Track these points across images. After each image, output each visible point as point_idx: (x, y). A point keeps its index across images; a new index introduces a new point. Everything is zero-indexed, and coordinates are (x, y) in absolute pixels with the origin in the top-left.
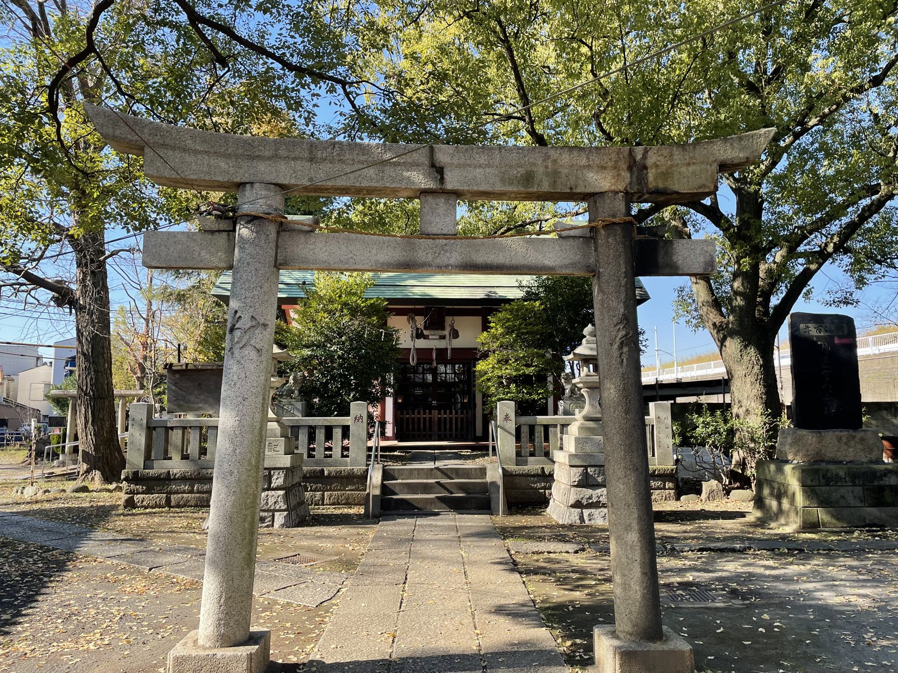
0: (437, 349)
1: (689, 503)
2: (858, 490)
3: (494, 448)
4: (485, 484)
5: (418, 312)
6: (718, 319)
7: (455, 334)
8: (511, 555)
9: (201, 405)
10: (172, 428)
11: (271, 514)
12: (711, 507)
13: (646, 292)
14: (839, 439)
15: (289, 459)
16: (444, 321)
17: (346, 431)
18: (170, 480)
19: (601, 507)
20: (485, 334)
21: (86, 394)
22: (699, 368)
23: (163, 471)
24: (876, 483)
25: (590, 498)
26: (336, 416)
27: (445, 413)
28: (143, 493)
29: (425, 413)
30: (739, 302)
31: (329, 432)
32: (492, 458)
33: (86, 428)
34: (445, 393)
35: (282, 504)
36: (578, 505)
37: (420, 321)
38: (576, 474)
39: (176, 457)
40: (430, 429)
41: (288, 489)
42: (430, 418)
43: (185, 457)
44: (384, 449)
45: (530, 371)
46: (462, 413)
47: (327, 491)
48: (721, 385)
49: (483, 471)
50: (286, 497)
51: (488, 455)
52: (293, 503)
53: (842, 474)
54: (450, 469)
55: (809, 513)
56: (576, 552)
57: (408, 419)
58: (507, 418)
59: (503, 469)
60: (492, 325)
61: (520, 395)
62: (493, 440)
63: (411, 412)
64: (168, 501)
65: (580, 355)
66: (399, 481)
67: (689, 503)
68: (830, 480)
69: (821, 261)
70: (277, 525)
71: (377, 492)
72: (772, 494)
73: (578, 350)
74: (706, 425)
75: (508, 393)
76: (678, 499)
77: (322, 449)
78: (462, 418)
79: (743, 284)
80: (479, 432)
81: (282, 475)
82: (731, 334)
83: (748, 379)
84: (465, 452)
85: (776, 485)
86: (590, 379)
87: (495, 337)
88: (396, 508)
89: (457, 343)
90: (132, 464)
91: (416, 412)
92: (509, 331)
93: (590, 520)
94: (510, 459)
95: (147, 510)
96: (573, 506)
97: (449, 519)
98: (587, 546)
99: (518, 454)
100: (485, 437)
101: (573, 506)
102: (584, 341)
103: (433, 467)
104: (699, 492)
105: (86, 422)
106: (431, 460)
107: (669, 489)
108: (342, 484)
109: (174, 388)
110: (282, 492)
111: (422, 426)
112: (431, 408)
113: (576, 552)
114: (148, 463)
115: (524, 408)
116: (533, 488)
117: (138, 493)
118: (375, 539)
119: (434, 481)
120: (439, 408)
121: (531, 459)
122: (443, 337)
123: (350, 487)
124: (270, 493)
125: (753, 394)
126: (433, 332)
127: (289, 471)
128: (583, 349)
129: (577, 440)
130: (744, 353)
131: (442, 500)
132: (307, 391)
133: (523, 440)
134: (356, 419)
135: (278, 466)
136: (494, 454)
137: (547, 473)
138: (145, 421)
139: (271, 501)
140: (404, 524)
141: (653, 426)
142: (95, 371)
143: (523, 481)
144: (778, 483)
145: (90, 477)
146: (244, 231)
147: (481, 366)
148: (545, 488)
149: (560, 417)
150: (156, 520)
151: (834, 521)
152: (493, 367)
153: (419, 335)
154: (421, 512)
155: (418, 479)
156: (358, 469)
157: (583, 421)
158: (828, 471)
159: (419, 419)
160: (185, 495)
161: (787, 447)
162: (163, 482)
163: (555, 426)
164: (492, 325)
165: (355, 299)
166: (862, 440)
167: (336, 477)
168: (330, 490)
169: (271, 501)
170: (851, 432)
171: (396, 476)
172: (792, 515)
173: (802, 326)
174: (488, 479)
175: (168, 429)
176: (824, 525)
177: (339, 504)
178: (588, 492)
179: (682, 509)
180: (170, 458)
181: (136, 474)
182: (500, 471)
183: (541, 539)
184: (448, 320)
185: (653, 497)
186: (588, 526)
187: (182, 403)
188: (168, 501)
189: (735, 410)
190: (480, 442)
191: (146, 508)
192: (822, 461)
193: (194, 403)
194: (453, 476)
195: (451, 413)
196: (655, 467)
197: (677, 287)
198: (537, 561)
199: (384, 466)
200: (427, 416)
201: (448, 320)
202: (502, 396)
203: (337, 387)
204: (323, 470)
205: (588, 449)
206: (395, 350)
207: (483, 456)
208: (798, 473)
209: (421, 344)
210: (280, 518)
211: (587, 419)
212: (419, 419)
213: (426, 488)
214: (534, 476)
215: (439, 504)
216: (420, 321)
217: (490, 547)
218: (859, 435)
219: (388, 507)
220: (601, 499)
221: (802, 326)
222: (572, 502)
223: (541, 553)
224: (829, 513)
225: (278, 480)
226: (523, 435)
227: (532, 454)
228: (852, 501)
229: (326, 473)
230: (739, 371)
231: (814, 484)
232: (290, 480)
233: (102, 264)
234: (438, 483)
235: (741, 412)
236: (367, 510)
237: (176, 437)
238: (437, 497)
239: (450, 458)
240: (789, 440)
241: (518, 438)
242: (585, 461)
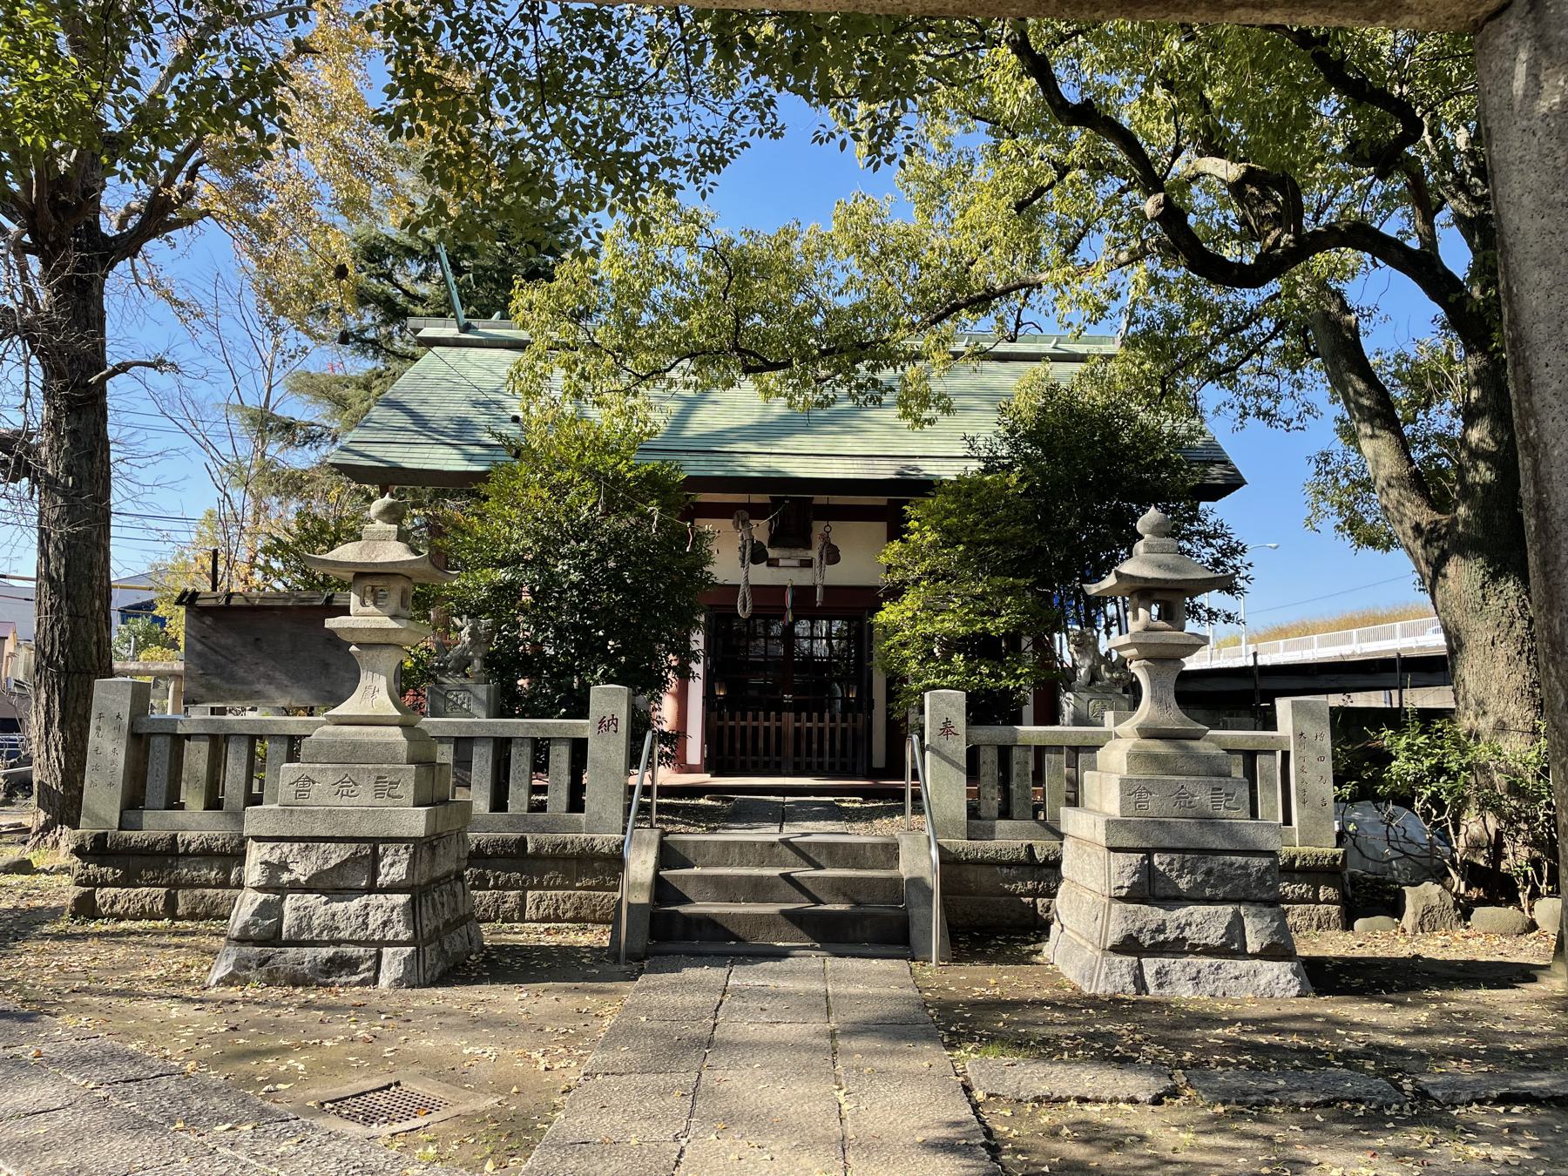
0: (794, 588)
1: (1372, 939)
3: (917, 796)
4: (896, 882)
5: (757, 512)
6: (1426, 516)
7: (832, 556)
8: (975, 1107)
9: (258, 687)
10: (188, 737)
11: (373, 951)
12: (1433, 947)
13: (1235, 470)
15: (423, 817)
16: (810, 530)
17: (579, 749)
18: (178, 856)
19: (1186, 954)
20: (897, 545)
21: (50, 664)
22: (1322, 644)
23: (162, 834)
25: (1161, 929)
26: (565, 716)
27: (809, 719)
28: (114, 884)
29: (767, 719)
30: (1483, 474)
31: (540, 751)
32: (909, 819)
33: (47, 734)
34: (813, 682)
35: (400, 927)
36: (1129, 946)
37: (761, 530)
38: (1124, 869)
39: (192, 798)
40: (778, 753)
41: (418, 892)
42: (779, 729)
45: (995, 626)
46: (844, 720)
47: (533, 888)
48: (1432, 669)
49: (890, 852)
50: (413, 909)
51: (901, 811)
52: (428, 925)
54: (816, 844)
56: (1157, 1101)
57: (732, 728)
58: (947, 729)
59: (940, 847)
60: (913, 524)
61: (975, 680)
62: (915, 776)
63: (738, 714)
64: (171, 903)
65: (1132, 577)
66: (696, 870)
67: (1372, 939)
70: (384, 981)
71: (643, 898)
73: (1127, 568)
74: (1414, 752)
75: (947, 673)
76: (1348, 926)
77: (524, 793)
78: (844, 730)
79: (1492, 432)
80: (879, 759)
81: (405, 856)
82: (1464, 546)
86: (1155, 638)
87: (917, 553)
88: (687, 937)
89: (838, 575)
90: (95, 817)
91: (750, 714)
92: (950, 537)
93: (1160, 986)
94: (954, 822)
95: (122, 925)
96: (1117, 949)
97: (811, 972)
98: (1180, 1078)
99: (973, 812)
100: (895, 766)
101: (1117, 949)
102: (1139, 547)
103: (775, 838)
105: (49, 722)
106: (773, 820)
107: (1327, 901)
108: (567, 874)
109: (199, 647)
110: (401, 899)
111: (761, 744)
112: (780, 707)
113: (1157, 1101)
114: (131, 815)
115: (987, 708)
116: (1007, 893)
117: (104, 885)
118: (615, 1037)
119: (776, 872)
120: (797, 708)
121: (1002, 825)
122: (807, 564)
123: (585, 882)
124: (374, 899)
125: (1513, 684)
126: (786, 553)
127: (423, 847)
128: (1138, 565)
129: (1125, 784)
130: (1490, 591)
132: (503, 665)
133: (984, 780)
135: (396, 833)
136: (918, 810)
137: (1040, 857)
138: (126, 720)
139: (375, 919)
140: (698, 986)
141: (1286, 755)
142: (70, 615)
143: (983, 877)
145: (50, 840)
147: (888, 614)
148: (1035, 894)
149: (1065, 730)
150: (119, 953)
152: (914, 618)
153: (757, 555)
154: (742, 949)
155: (741, 865)
156: (604, 840)
157: (1136, 740)
159: (755, 729)
160: (209, 892)
162: (158, 861)
163: (1058, 749)
164: (913, 524)
165: (611, 461)
167: (553, 858)
168: (539, 887)
169: (375, 919)
171: (691, 857)
174: (905, 870)
175: (178, 740)
177: (558, 919)
178: (1156, 914)
179: (1366, 953)
180: (181, 807)
181: (100, 839)
182: (934, 853)
183: (1047, 1049)
184: (818, 527)
185: (1290, 920)
186: (1156, 1004)
187: (216, 681)
188: (171, 903)
189: (1465, 723)
190: (884, 781)
191: (120, 918)
193: (243, 682)
194: (822, 860)
195: (821, 719)
196: (1293, 850)
197: (1314, 452)
198: (1054, 1133)
199: (664, 833)
200: (772, 724)
201: (818, 527)
202: (933, 680)
203: (567, 653)
204: (523, 842)
205: (1155, 805)
206: (706, 582)
207: (890, 813)
209: (762, 575)
210: (393, 964)
211: (1148, 733)
212: (755, 729)
213: (758, 889)
214: (1010, 864)
215: (787, 928)
216: (761, 530)
217: (916, 1076)
219: (670, 934)
220: (1187, 933)
222: (1114, 937)
223: (1060, 1100)
225: (394, 868)
226: (983, 770)
227: (1005, 814)
229: (530, 847)
230: (1479, 632)
232: (424, 867)
233: (98, 394)
234: (786, 877)
235: (1485, 725)
236: (615, 933)
237: (196, 757)
238: (783, 913)
239: (816, 817)
241: (973, 771)
242: (1147, 838)
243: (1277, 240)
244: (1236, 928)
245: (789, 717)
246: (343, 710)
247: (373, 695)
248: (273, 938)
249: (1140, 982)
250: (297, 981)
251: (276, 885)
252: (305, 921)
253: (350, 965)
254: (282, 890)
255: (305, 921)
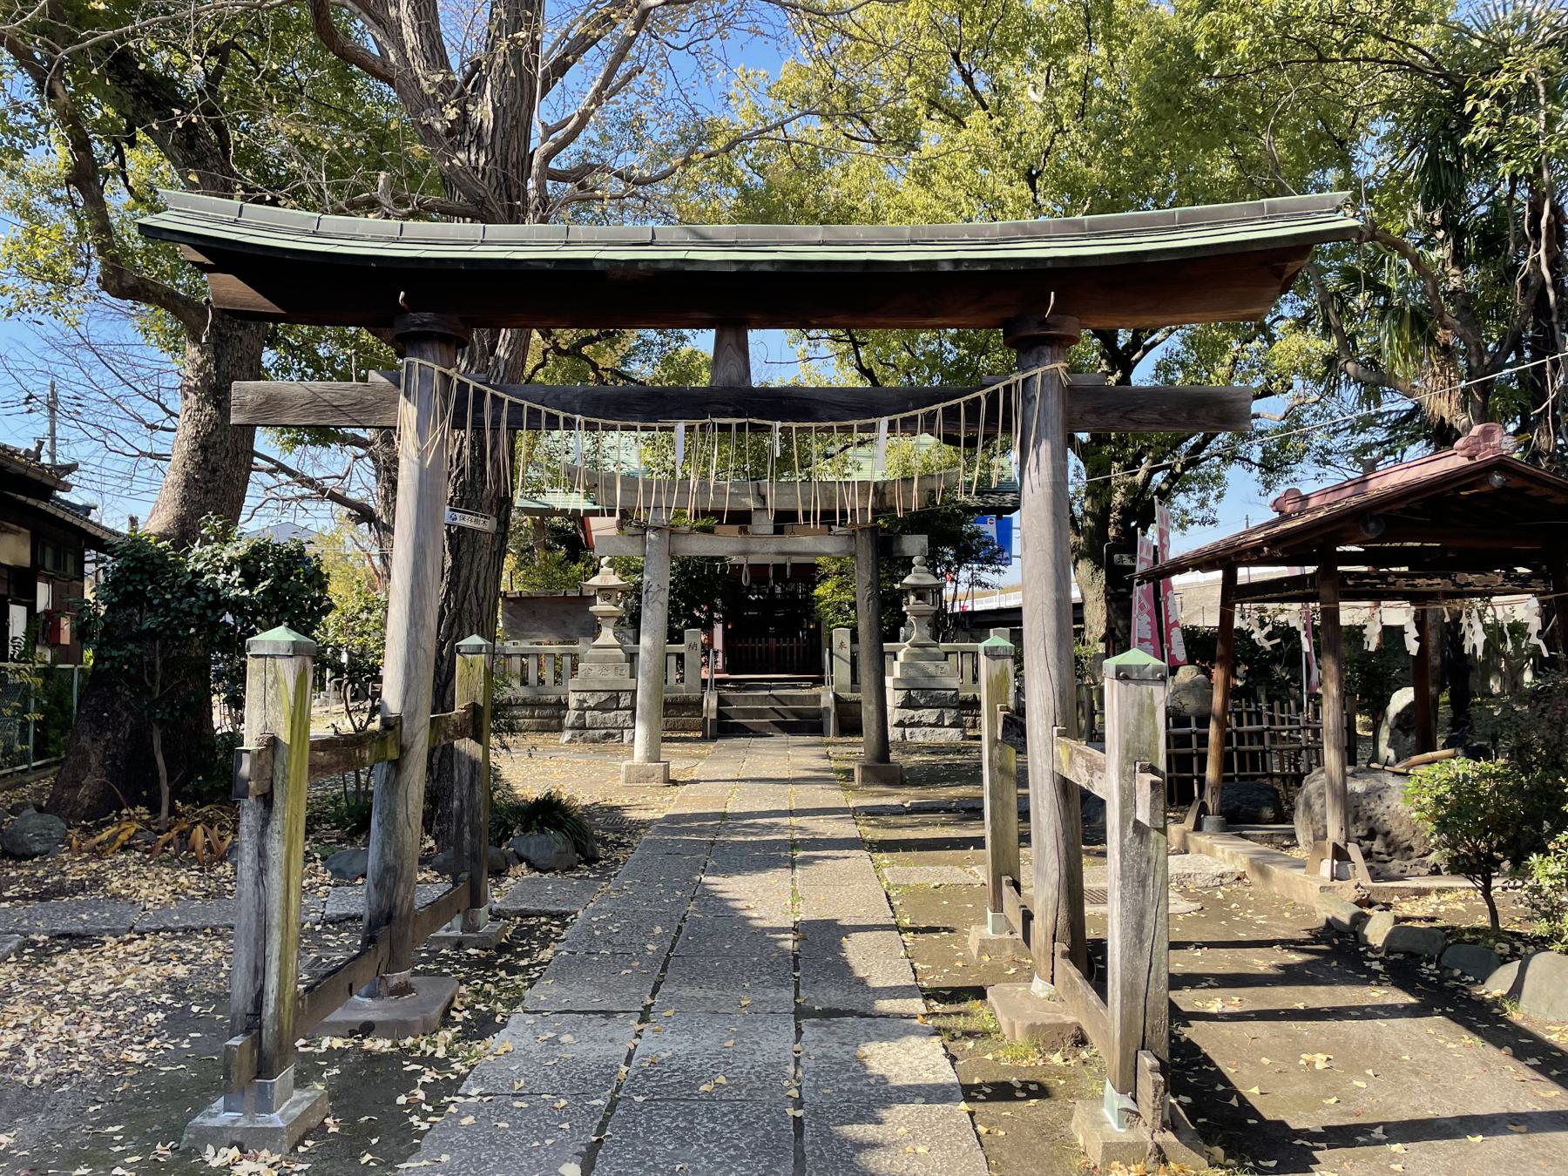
10: (510, 656)
39: (516, 684)
43: (524, 682)
44: (718, 681)
49: (817, 698)
71: (714, 716)
82: (1082, 556)
84: (804, 684)
120: (777, 636)
131: (776, 724)
134: (692, 647)
139: (620, 720)
146: (651, 535)
169: (620, 720)
173: (1116, 556)
178: (912, 712)
213: (760, 713)
243: (1476, 37)
244: (941, 717)
245: (773, 641)
246: (597, 642)
247: (607, 636)
248: (583, 727)
249: (904, 736)
250: (594, 741)
251: (582, 708)
252: (594, 719)
253: (613, 736)
254: (585, 710)
255: (594, 719)
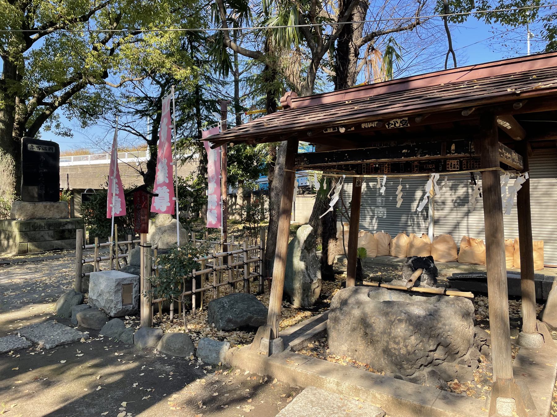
2: (51, 232)
14: (45, 207)
22: (75, 160)
24: (61, 228)
53: (43, 224)
55: (22, 245)
68: (35, 228)
69: (52, 110)
72: (5, 238)
83: (5, 173)
85: (7, 232)
104: (301, 260)
125: (8, 182)
144: (9, 231)
151: (36, 249)
158: (35, 223)
161: (16, 211)
166: (58, 207)
170: (52, 203)
172: (14, 247)
173: (29, 145)
176: (31, 251)
192: (34, 218)
208: (18, 225)
218: (56, 204)
221: (29, 145)
224: (33, 245)
228: (47, 238)
231: (26, 230)
240: (17, 208)
